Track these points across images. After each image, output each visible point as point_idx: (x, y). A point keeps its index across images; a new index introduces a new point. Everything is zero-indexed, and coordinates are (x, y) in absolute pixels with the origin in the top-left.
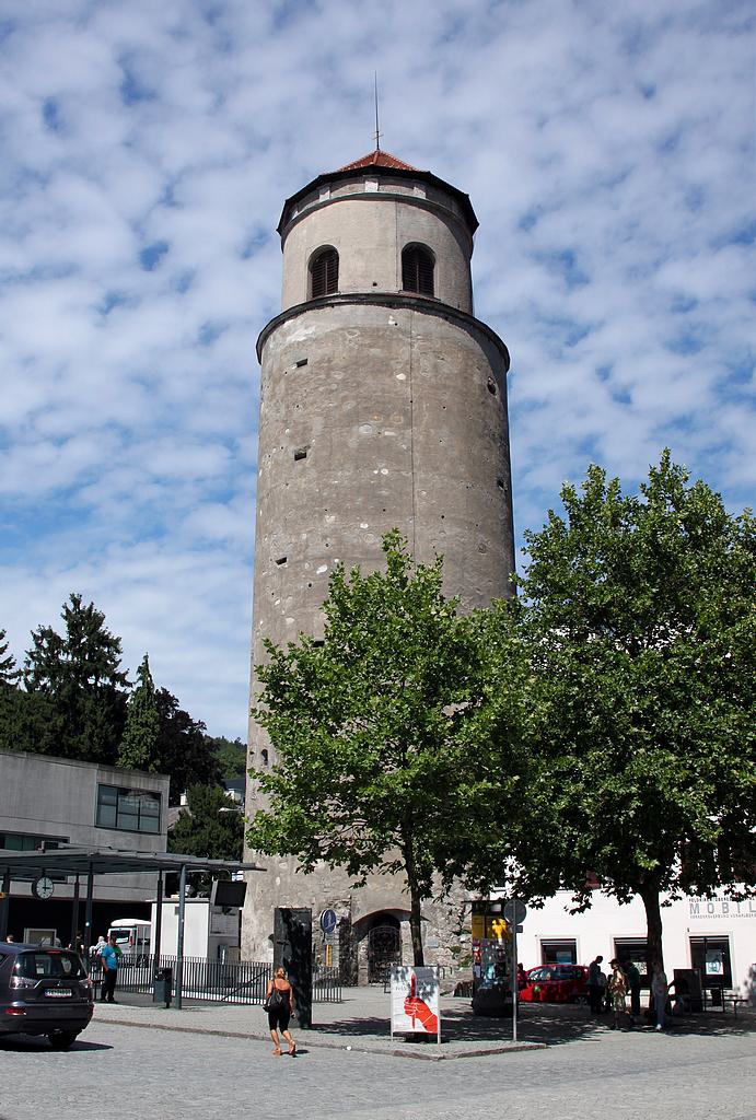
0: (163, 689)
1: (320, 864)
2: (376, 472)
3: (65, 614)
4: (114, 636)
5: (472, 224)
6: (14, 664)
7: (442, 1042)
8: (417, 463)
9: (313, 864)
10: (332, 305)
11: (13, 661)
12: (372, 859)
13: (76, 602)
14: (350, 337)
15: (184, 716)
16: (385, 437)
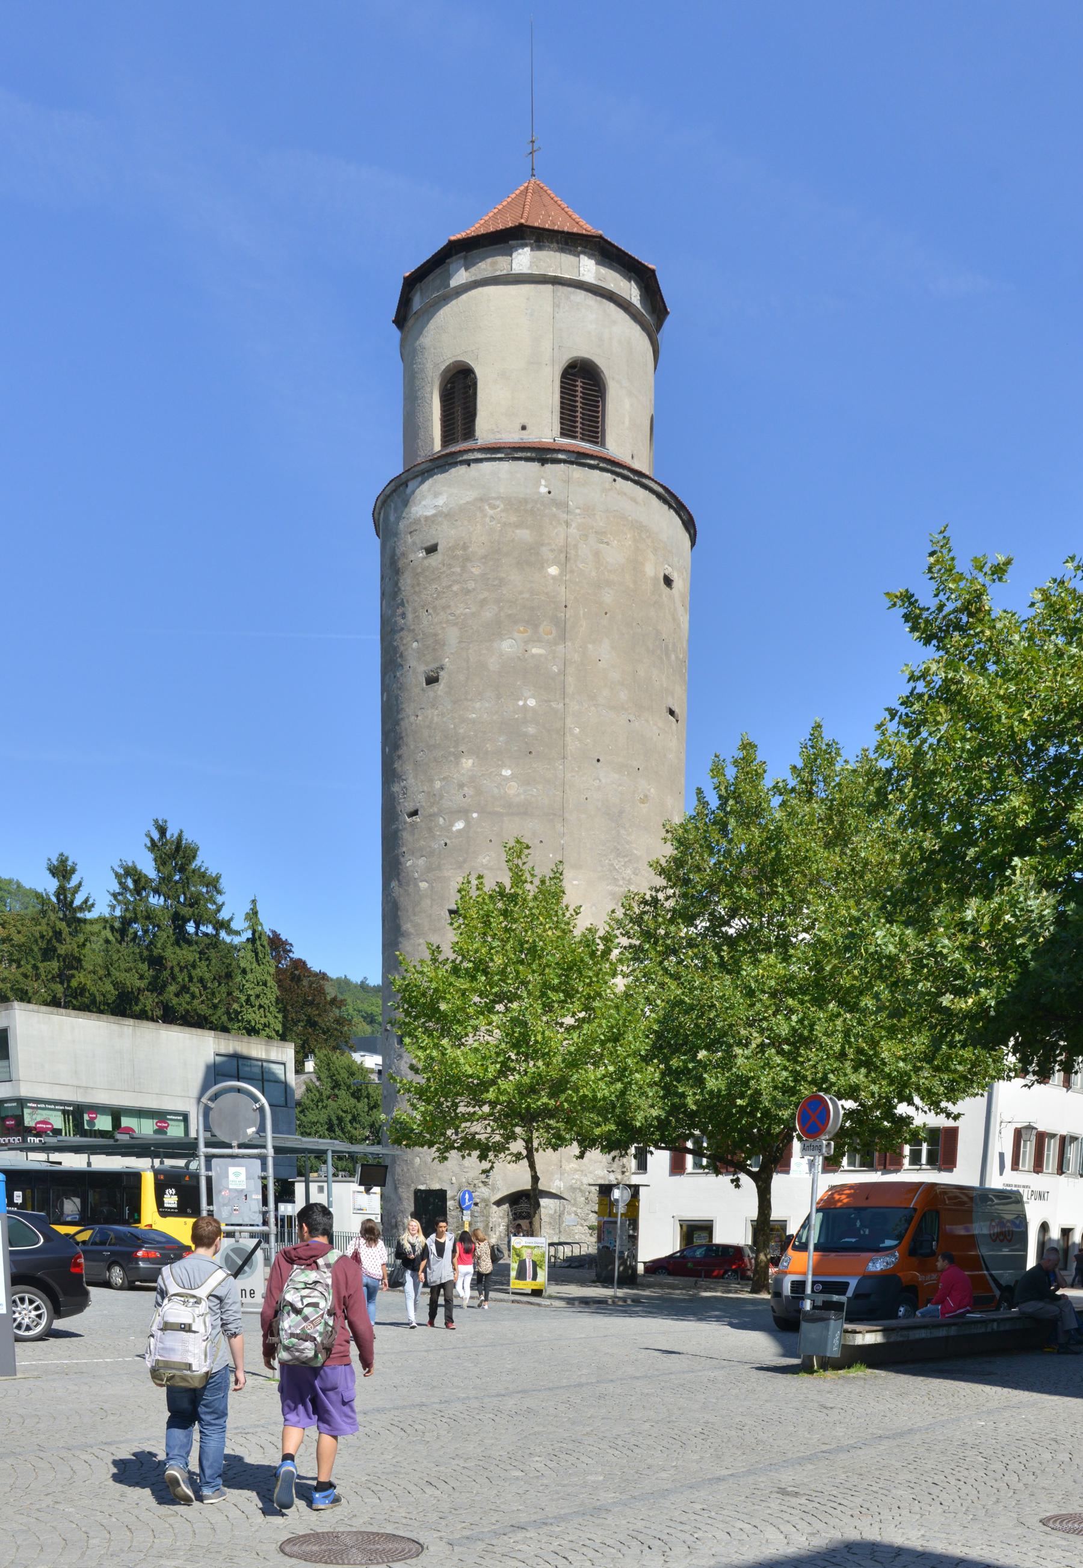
0: (274, 932)
1: (453, 1154)
2: (521, 703)
3: (149, 844)
4: (213, 872)
5: (666, 312)
6: (93, 905)
7: (325, 1152)
8: (570, 690)
9: (447, 1154)
10: (468, 463)
11: (90, 902)
12: (500, 1148)
13: (162, 831)
15: (300, 964)
16: (533, 656)
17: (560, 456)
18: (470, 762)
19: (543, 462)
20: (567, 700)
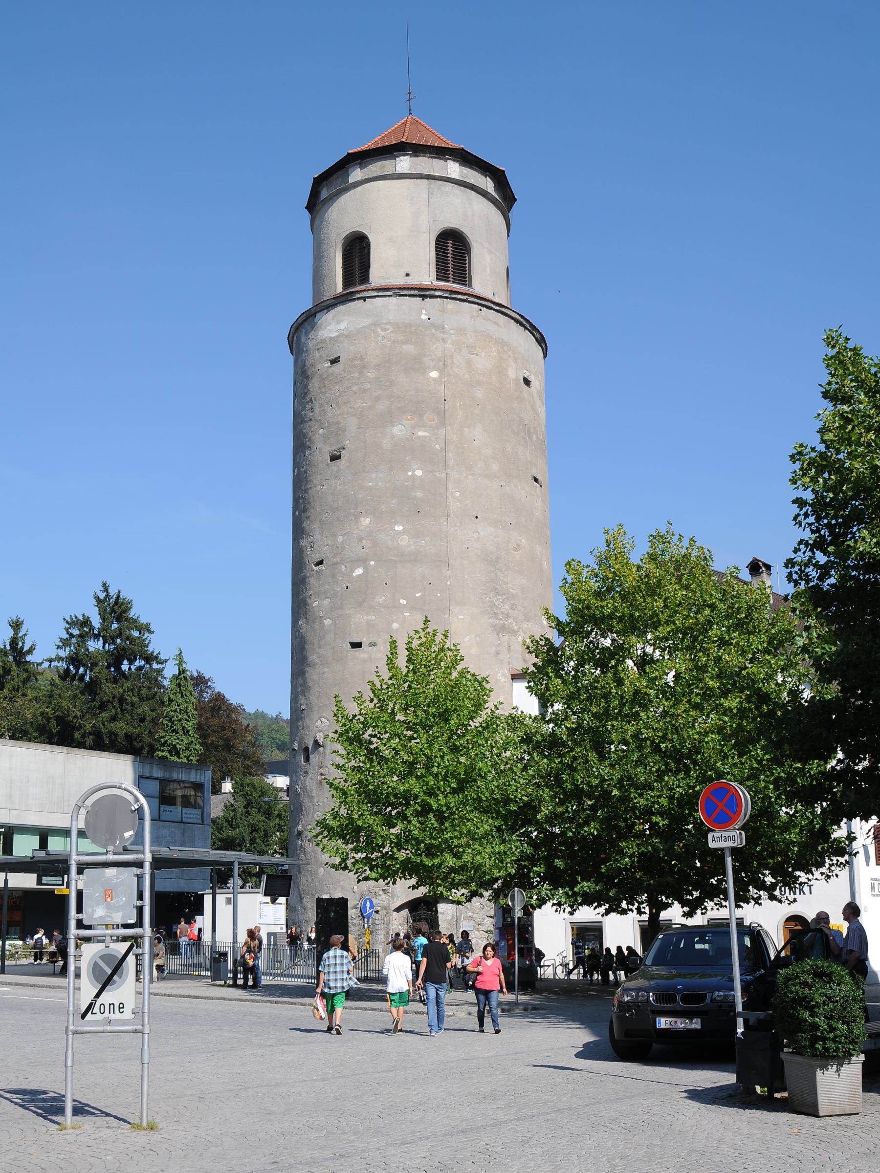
2: (410, 473)
4: (143, 620)
8: (451, 463)
10: (364, 299)
14: (383, 333)
15: (219, 698)
16: (419, 437)
17: (437, 293)
18: (368, 520)
19: (424, 297)
20: (448, 471)
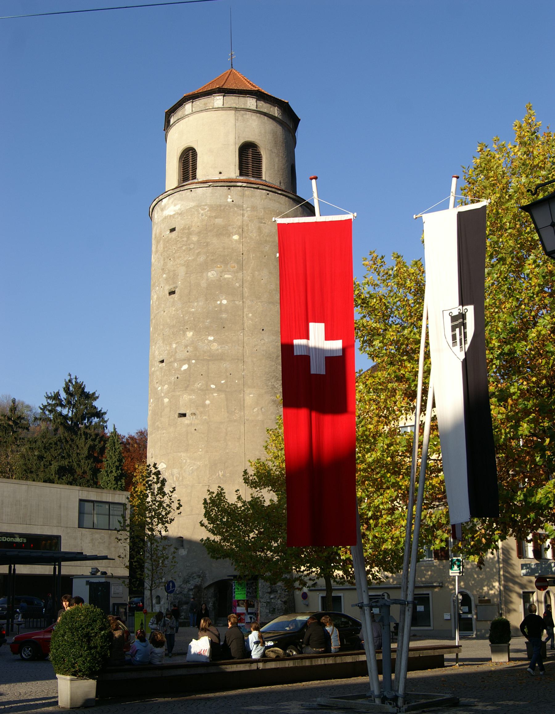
2: (219, 302)
8: (246, 295)
20: (244, 300)
